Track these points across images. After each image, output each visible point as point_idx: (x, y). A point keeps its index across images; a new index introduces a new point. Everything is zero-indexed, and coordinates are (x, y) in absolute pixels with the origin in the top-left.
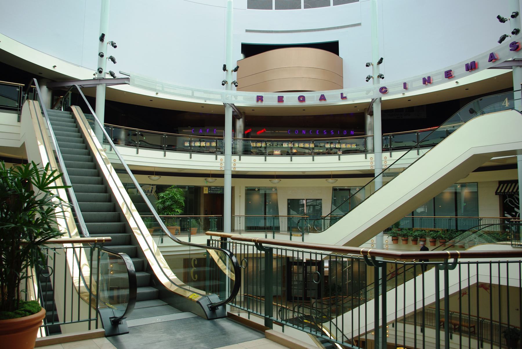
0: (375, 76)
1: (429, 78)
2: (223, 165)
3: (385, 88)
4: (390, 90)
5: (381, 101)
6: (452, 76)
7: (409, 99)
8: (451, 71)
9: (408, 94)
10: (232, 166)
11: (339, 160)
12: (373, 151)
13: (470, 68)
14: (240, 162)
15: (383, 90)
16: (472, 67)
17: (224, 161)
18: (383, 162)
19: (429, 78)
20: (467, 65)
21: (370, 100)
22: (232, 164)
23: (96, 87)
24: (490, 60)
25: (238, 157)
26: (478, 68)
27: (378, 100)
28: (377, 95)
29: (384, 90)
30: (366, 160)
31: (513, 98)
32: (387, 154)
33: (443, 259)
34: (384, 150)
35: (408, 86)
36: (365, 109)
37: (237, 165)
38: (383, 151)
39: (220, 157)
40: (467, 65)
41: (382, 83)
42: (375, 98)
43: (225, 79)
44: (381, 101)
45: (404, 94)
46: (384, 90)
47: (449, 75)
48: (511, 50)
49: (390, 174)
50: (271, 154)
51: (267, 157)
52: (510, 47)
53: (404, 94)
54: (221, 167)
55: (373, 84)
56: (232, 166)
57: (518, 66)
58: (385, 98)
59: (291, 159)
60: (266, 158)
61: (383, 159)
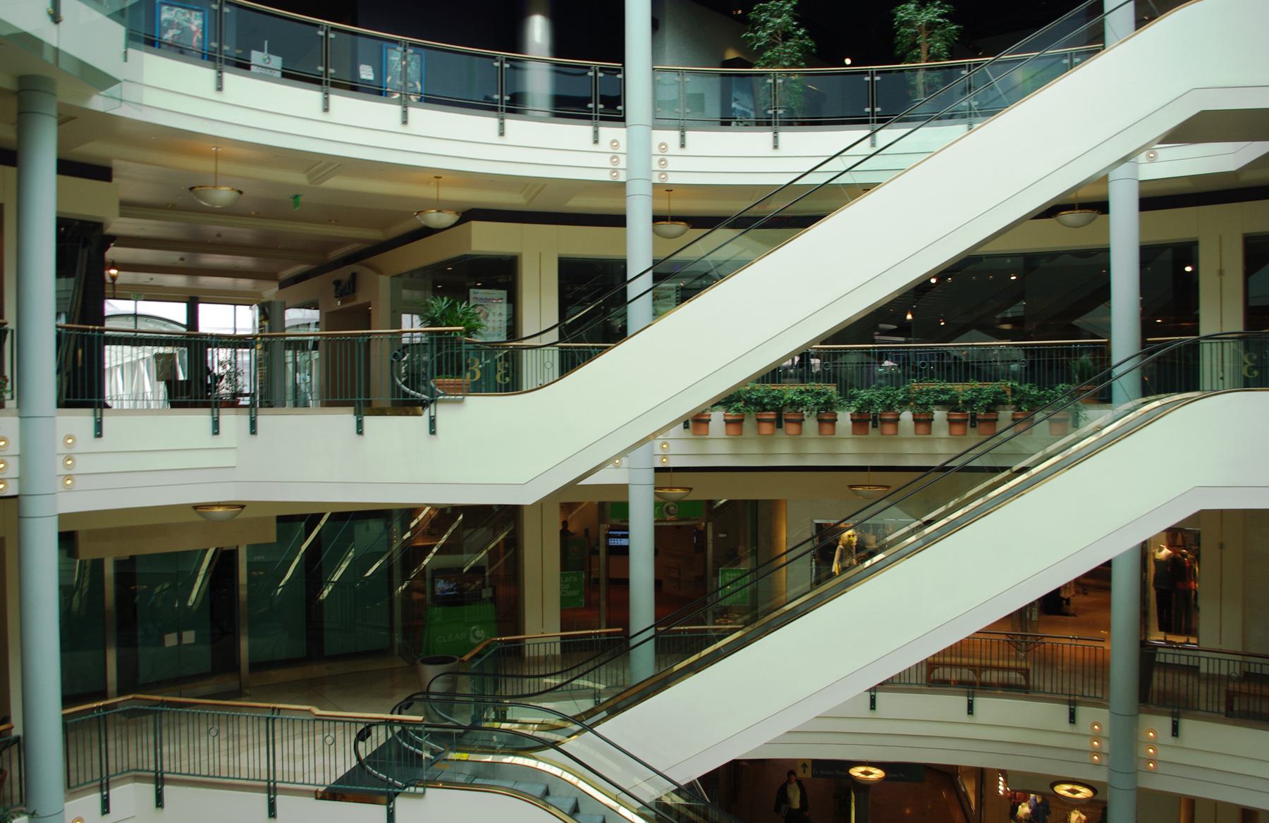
2: (623, 163)
10: (656, 166)
14: (683, 152)
17: (623, 149)
18: (655, 160)
22: (655, 160)
23: (1106, 707)
25: (676, 135)
30: (596, 148)
33: (195, 608)
37: (673, 164)
39: (609, 132)
43: (579, 817)
49: (785, 215)
50: (243, 65)
51: (689, 134)
54: (614, 170)
56: (656, 166)
60: (502, 125)
61: (656, 150)
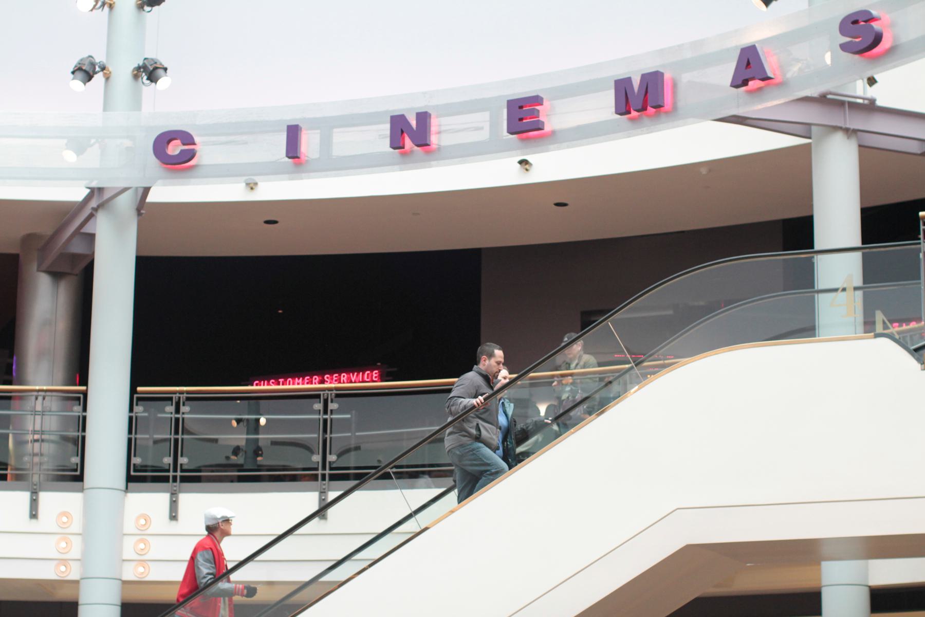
0: (122, 69)
1: (423, 118)
3: (187, 139)
4: (206, 154)
5: (142, 206)
6: (539, 127)
7: (562, 195)
8: (536, 100)
9: (553, 165)
11: (34, 515)
12: (73, 476)
13: (636, 102)
15: (175, 150)
16: (642, 99)
19: (423, 118)
20: (622, 88)
21: (77, 194)
24: (740, 82)
26: (675, 108)
27: (125, 203)
28: (122, 163)
29: (175, 149)
30: (34, 525)
31: (812, 285)
32: (152, 502)
34: (138, 476)
35: (309, 144)
36: (28, 240)
38: (130, 479)
40: (622, 88)
41: (164, 105)
42: (111, 182)
44: (142, 206)
45: (252, 186)
46: (175, 149)
47: (524, 119)
48: (844, 47)
52: (843, 29)
53: (252, 186)
55: (106, 107)
57: (836, 128)
58: (169, 192)
59: (174, 505)
